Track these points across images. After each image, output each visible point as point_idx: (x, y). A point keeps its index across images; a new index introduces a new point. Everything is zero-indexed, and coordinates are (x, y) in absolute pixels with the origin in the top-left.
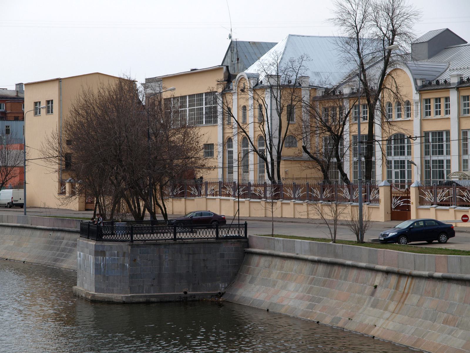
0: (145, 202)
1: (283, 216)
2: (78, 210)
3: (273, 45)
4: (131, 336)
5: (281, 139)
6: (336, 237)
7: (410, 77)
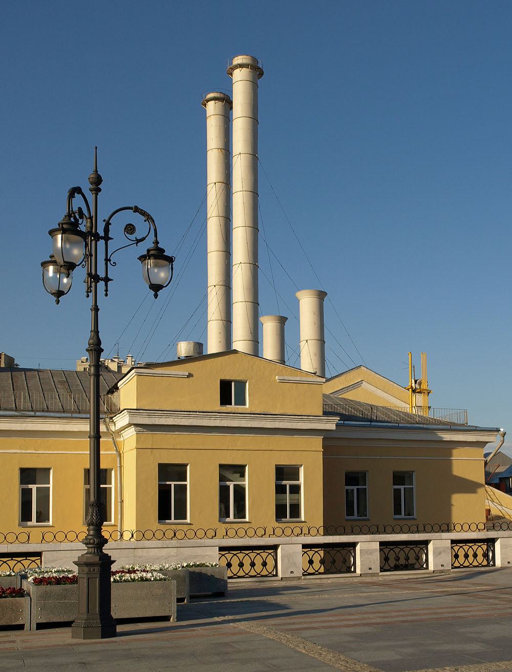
2: (102, 466)
5: (436, 610)
7: (335, 537)
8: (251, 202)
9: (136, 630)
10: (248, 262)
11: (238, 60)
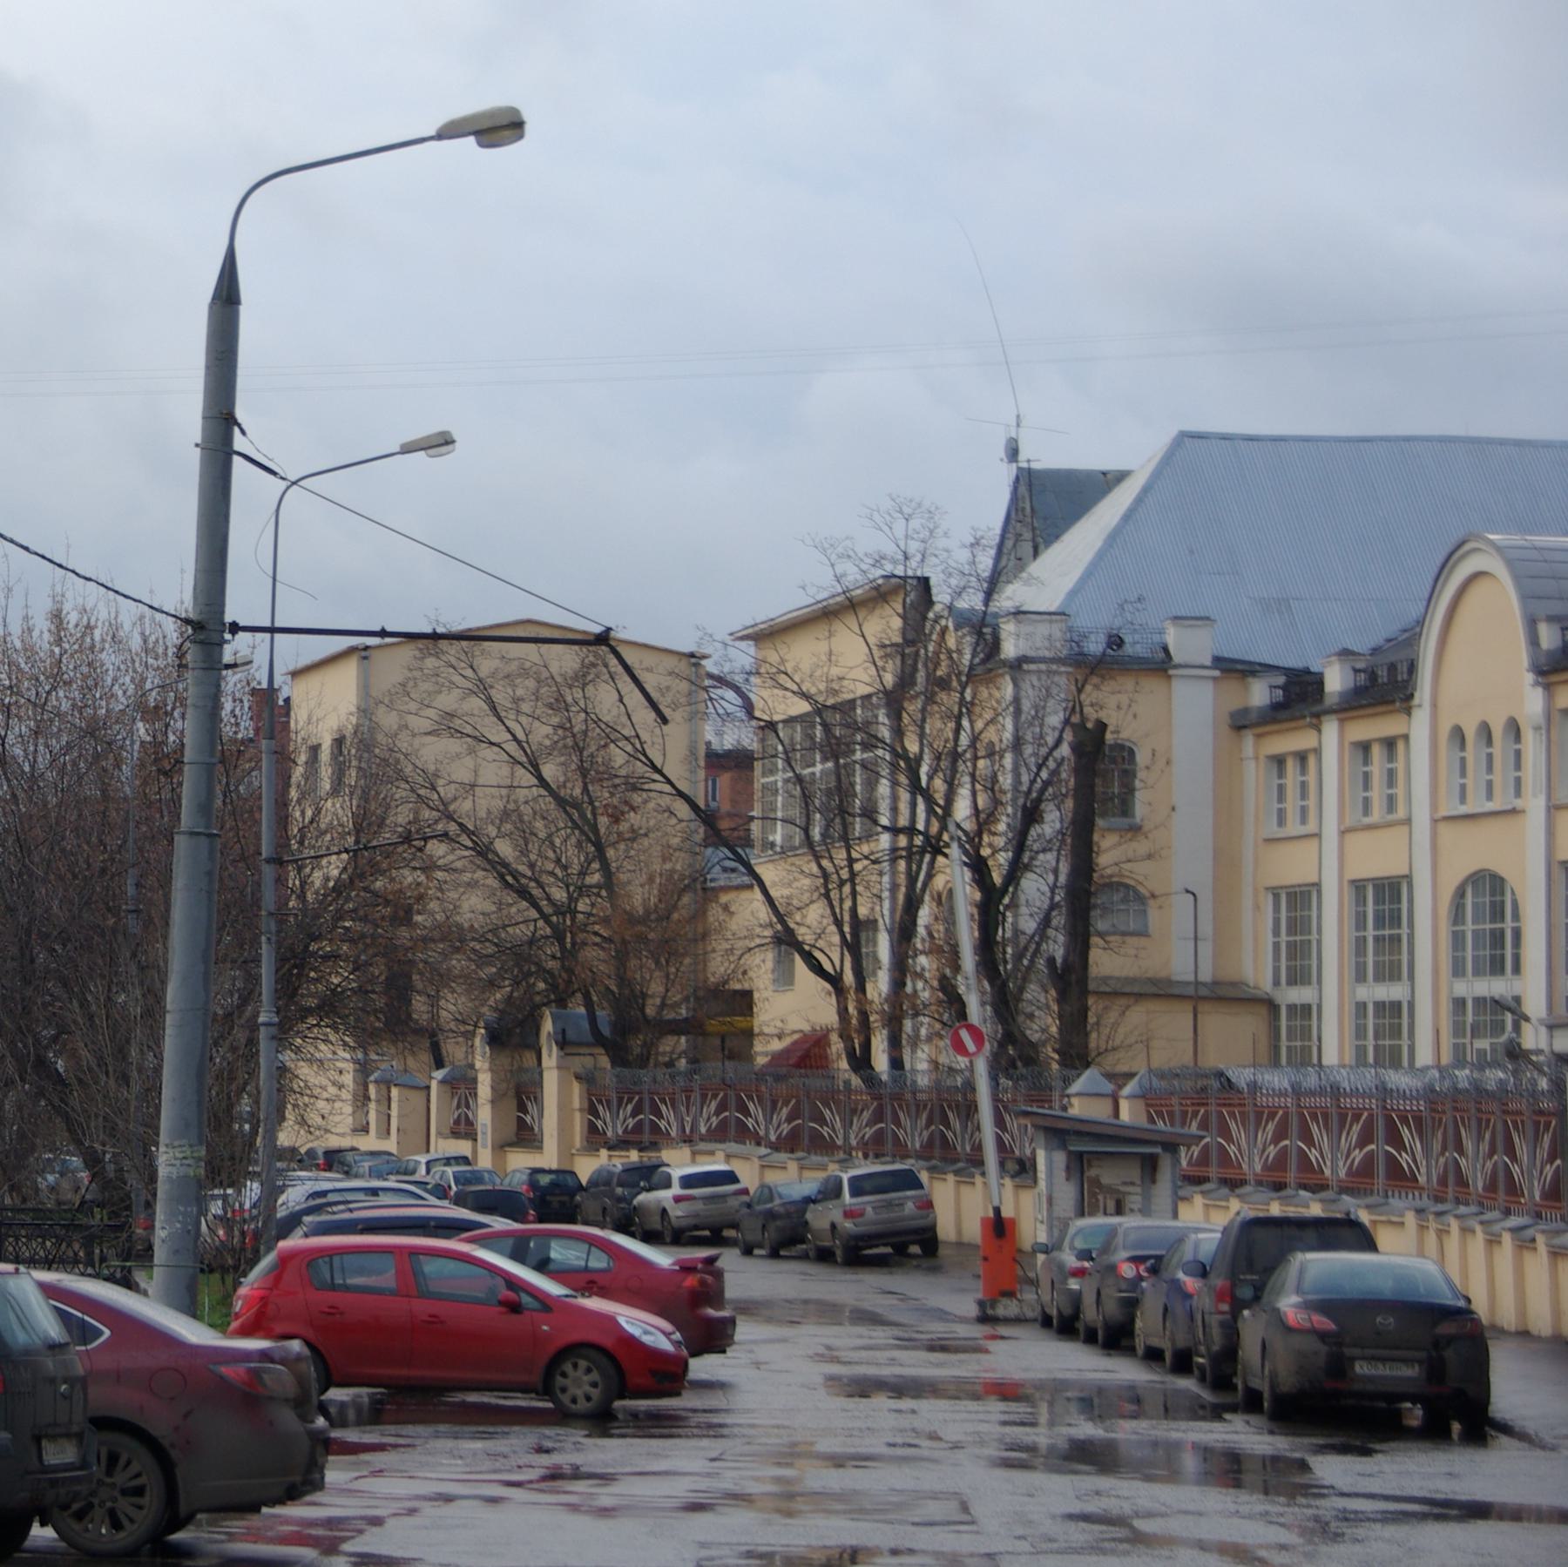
0: (612, 1402)
1: (587, 1246)
3: (1121, 476)
6: (45, 1457)
8: (1123, 1355)
11: (237, 1126)
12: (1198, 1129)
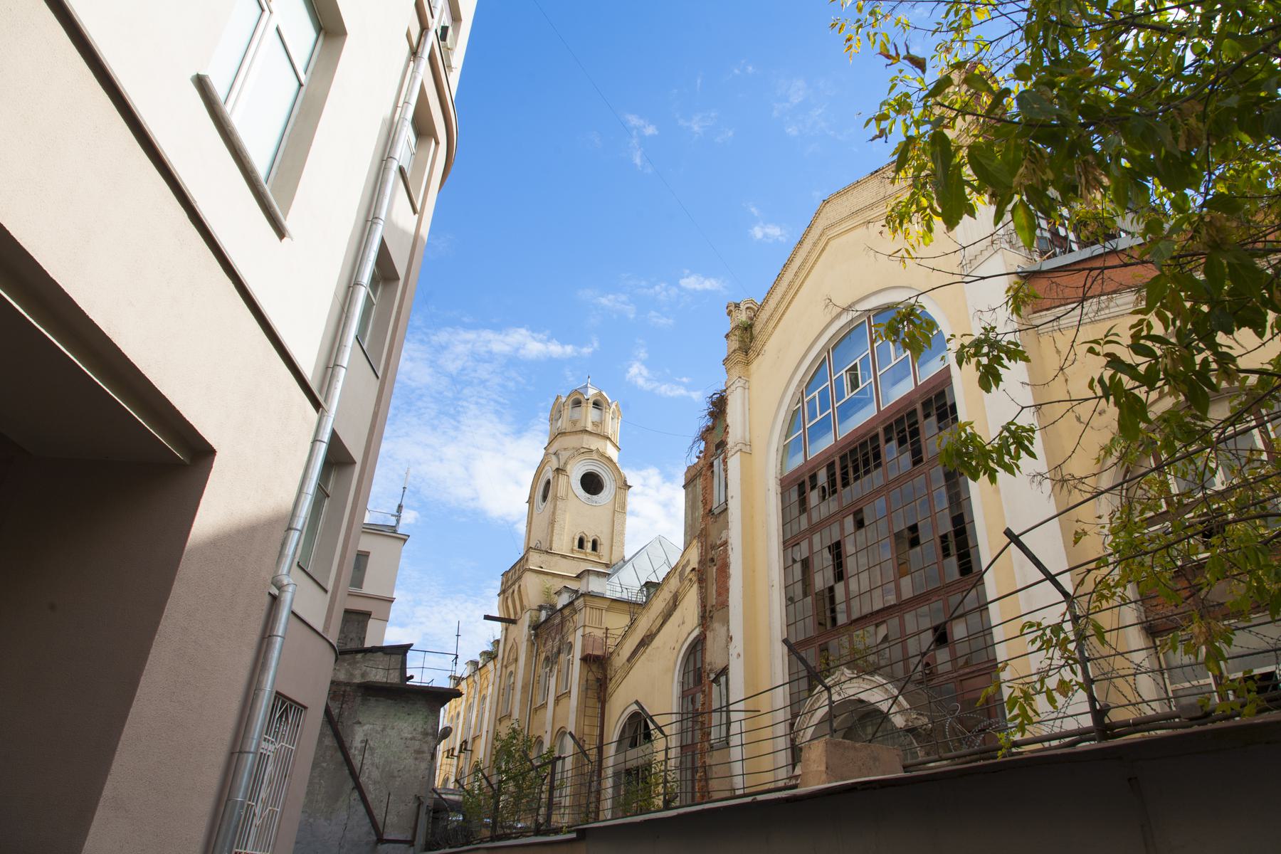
4: (720, 455)
9: (326, 326)
10: (1032, 404)
12: (1209, 677)
